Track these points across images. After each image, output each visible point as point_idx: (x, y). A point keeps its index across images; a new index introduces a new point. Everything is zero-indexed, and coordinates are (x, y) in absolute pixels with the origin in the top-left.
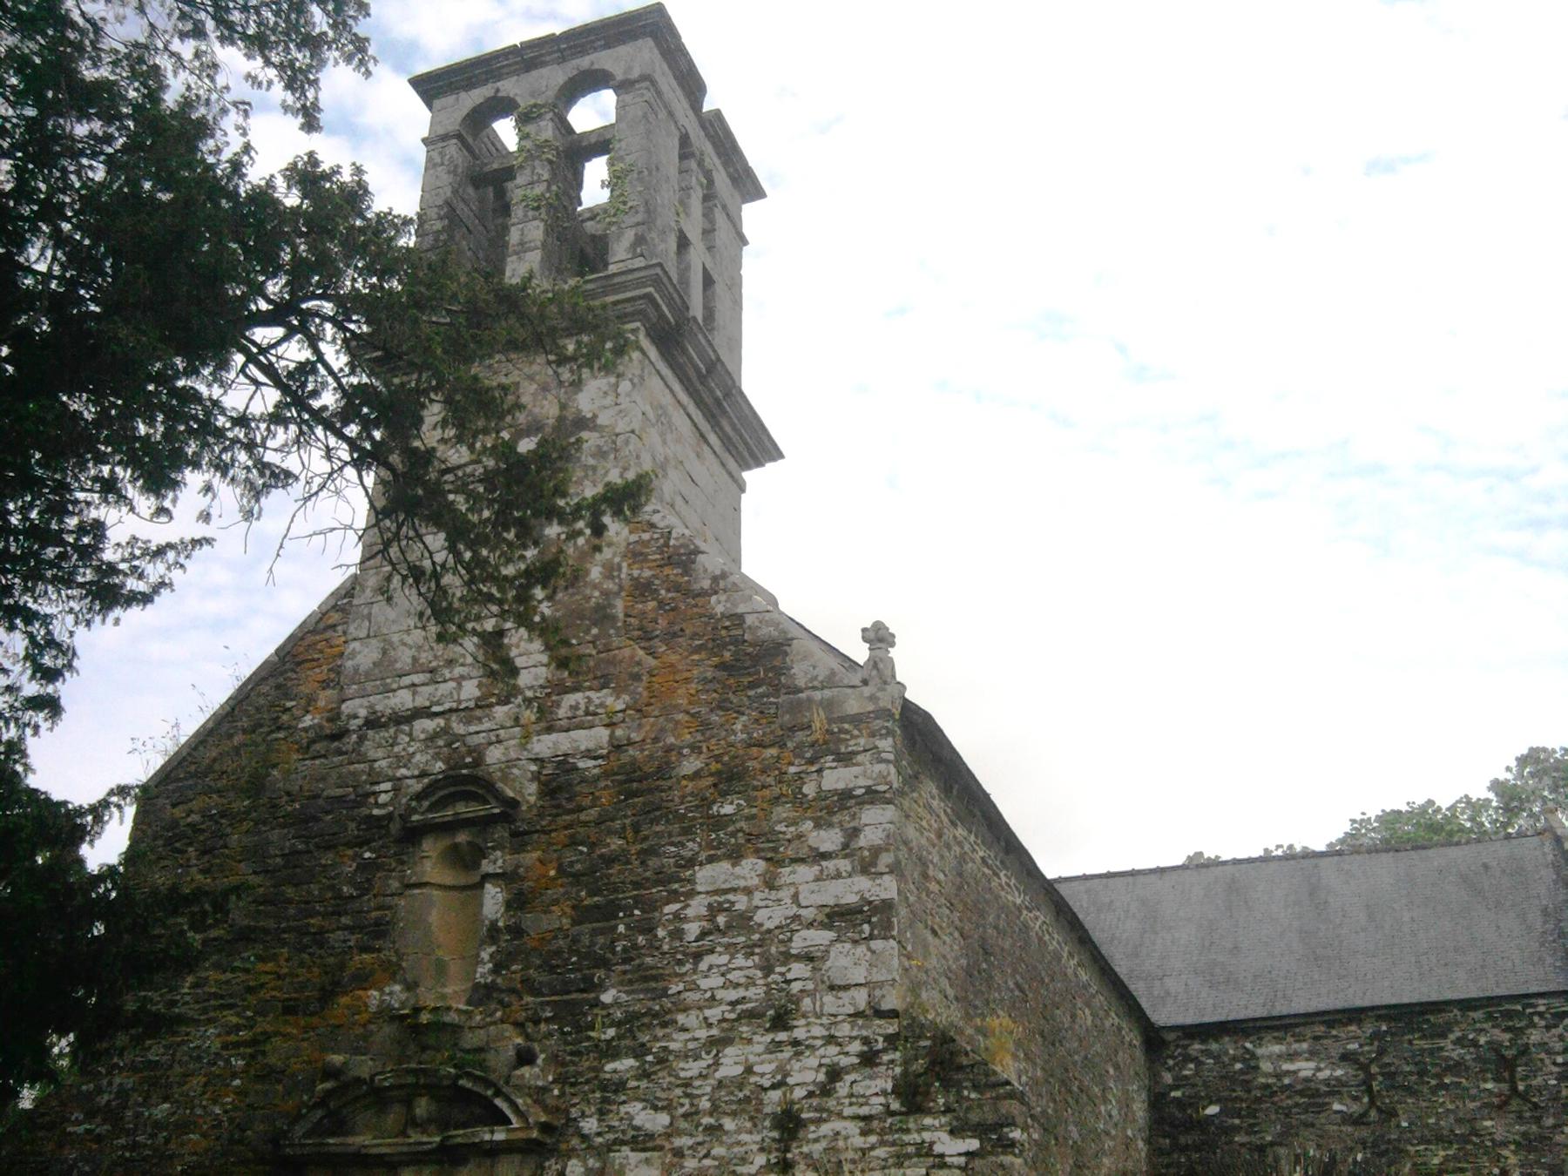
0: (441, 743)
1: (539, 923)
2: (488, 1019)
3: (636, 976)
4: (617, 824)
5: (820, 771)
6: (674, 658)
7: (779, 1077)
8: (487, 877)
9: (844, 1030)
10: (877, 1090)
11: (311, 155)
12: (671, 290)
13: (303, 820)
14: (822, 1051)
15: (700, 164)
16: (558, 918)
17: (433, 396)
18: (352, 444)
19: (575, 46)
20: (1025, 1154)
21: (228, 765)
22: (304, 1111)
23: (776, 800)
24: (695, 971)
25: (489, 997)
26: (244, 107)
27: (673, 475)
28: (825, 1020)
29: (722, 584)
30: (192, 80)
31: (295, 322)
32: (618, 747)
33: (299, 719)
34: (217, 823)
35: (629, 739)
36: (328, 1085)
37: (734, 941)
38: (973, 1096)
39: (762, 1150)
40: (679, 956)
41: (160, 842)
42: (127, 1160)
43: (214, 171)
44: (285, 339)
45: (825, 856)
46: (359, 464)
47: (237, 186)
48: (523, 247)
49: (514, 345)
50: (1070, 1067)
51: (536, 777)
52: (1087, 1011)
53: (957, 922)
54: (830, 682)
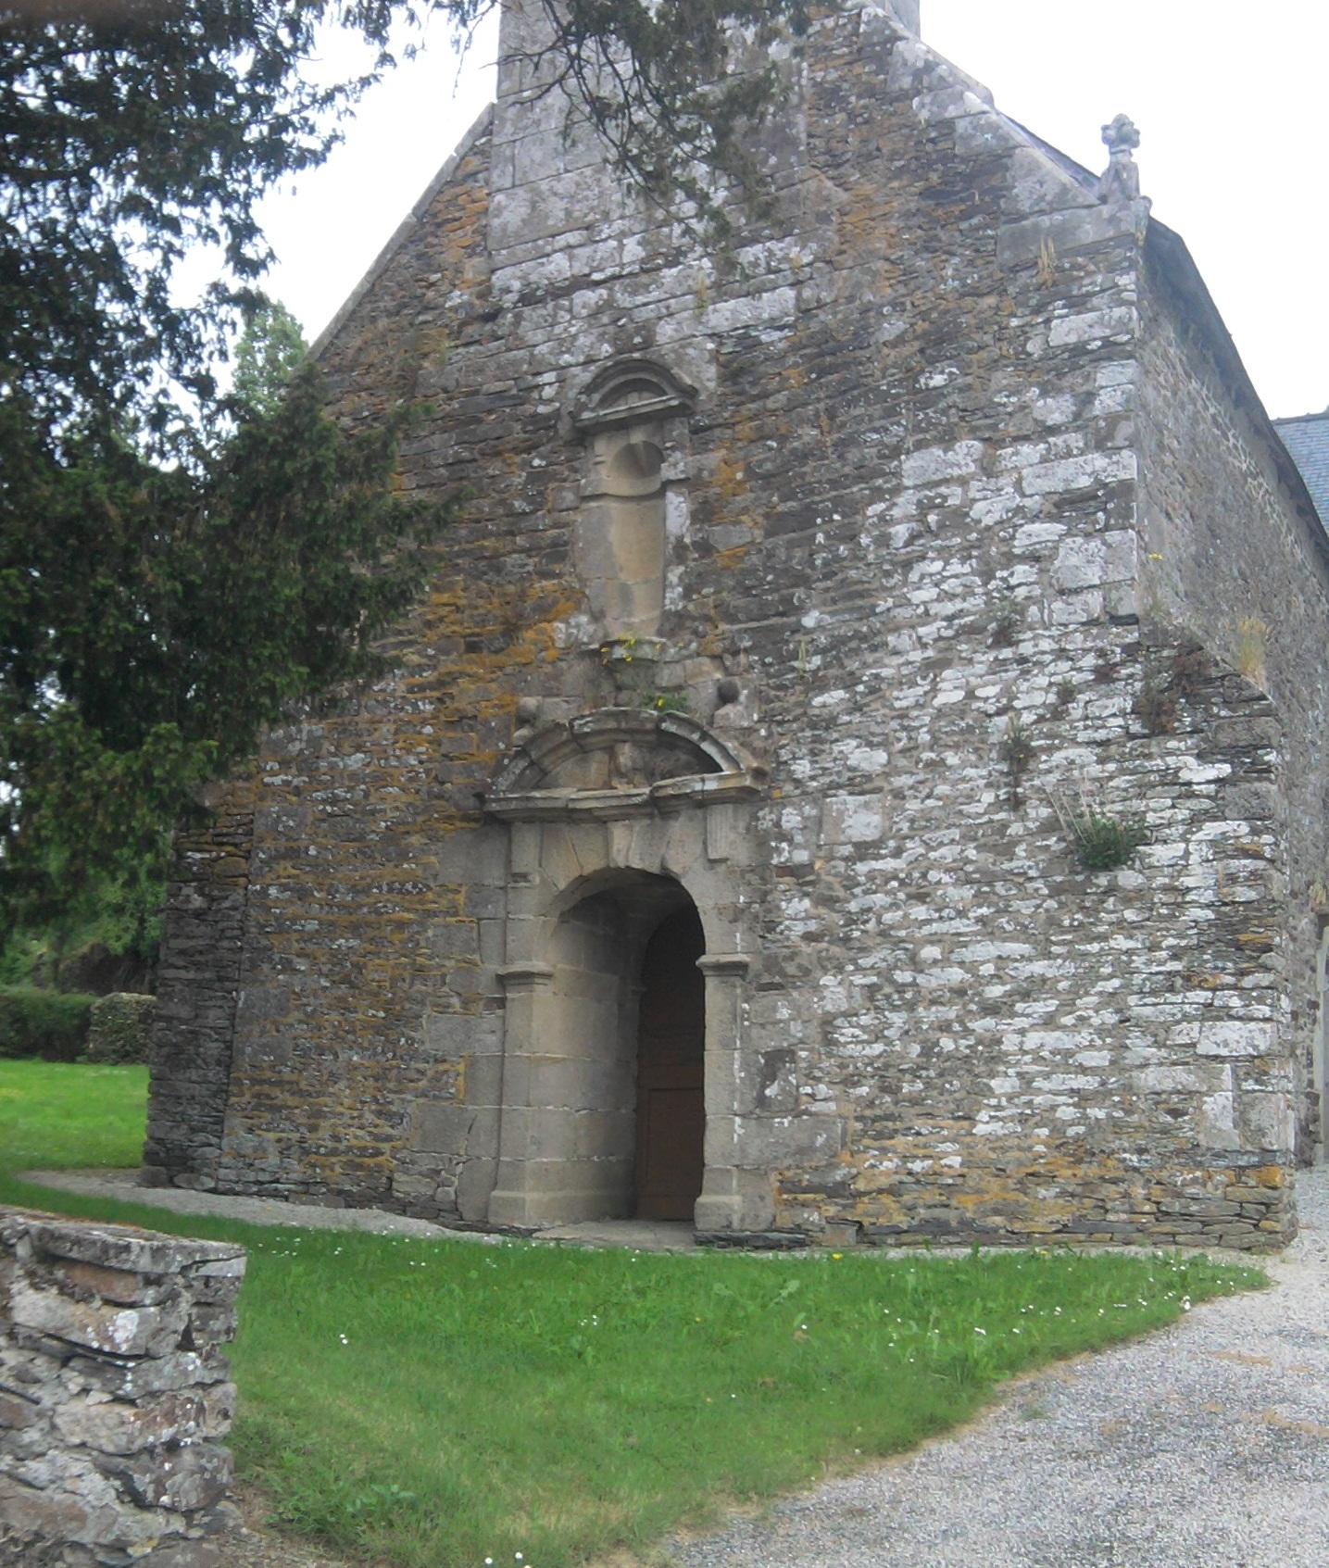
0: (605, 320)
5: (1047, 321)
6: (868, 188)
7: (1004, 701)
8: (667, 484)
10: (1114, 710)
13: (463, 423)
14: (1051, 668)
21: (373, 355)
23: (994, 365)
24: (905, 583)
25: (681, 626)
33: (445, 295)
35: (819, 300)
36: (524, 732)
38: (1223, 713)
39: (989, 785)
40: (886, 567)
42: (330, 815)
45: (1054, 430)
54: (1062, 200)
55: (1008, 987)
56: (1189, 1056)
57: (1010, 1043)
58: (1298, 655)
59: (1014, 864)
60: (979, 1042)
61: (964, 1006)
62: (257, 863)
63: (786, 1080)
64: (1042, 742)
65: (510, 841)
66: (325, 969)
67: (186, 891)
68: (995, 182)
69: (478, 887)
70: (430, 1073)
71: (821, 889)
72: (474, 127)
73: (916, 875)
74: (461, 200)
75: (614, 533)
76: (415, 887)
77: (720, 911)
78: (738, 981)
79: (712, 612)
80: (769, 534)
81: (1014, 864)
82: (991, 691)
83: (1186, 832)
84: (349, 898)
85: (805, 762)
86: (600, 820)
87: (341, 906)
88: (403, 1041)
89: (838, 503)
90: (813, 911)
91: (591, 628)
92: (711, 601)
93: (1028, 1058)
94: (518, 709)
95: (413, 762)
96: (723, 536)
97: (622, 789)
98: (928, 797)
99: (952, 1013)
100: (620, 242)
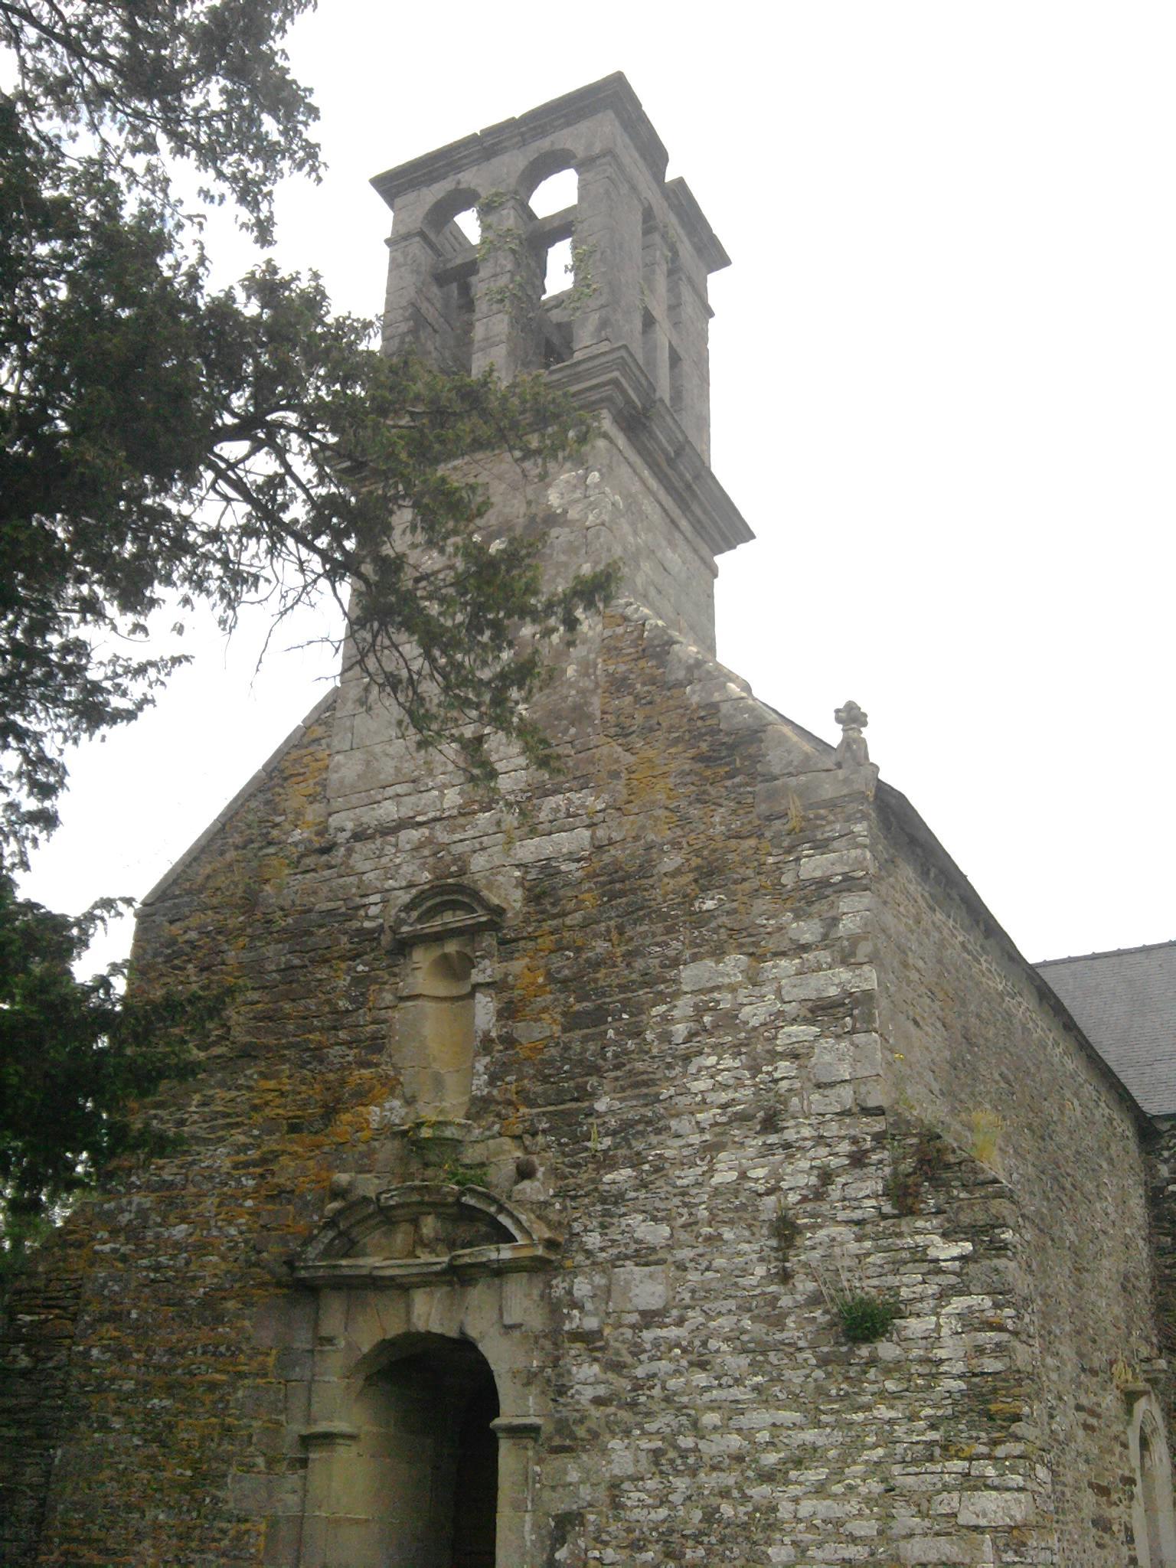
0: (426, 852)
1: (531, 1032)
2: (487, 1133)
3: (629, 1081)
4: (602, 927)
5: (798, 859)
6: (651, 753)
7: (773, 1182)
8: (476, 987)
9: (833, 1129)
10: (868, 1192)
11: (269, 262)
12: (638, 373)
13: (296, 935)
14: (811, 1153)
15: (664, 236)
16: (548, 1027)
17: (400, 502)
18: (326, 557)
19: (535, 128)
20: (1018, 1257)
21: (221, 881)
22: (315, 1232)
23: (755, 893)
24: (684, 1074)
25: (486, 1110)
26: (199, 220)
27: (646, 566)
28: (813, 1120)
29: (696, 674)
30: (146, 195)
31: (261, 435)
32: (600, 847)
33: (288, 833)
34: (214, 939)
35: (610, 839)
36: (335, 1205)
37: (721, 1041)
38: (962, 1195)
39: (761, 1260)
40: (669, 1060)
41: (160, 960)
42: (153, 1281)
43: (172, 285)
44: (253, 451)
45: (805, 948)
46: (334, 573)
47: (195, 299)
48: (489, 342)
49: (478, 445)
50: (1062, 1162)
51: (520, 883)
52: (1076, 1103)
53: (939, 1012)
54: (806, 766)
55: (782, 1455)
56: (951, 1527)
57: (785, 1511)
58: (1078, 1153)
59: (785, 1335)
60: (756, 1509)
61: (742, 1472)
62: (82, 1325)
63: (576, 1544)
64: (805, 1220)
65: (318, 1309)
66: (138, 1429)
67: (15, 1351)
68: (752, 750)
69: (287, 1350)
70: (232, 1533)
71: (610, 1355)
72: (320, 704)
73: (697, 1343)
74: (305, 760)
75: (430, 1029)
76: (228, 1349)
77: (515, 1374)
78: (530, 1444)
79: (514, 1097)
80: (566, 1030)
81: (785, 1335)
82: (760, 1173)
83: (937, 1306)
84: (165, 1360)
85: (596, 1234)
86: (402, 1287)
87: (158, 1368)
88: (208, 1500)
89: (625, 1004)
90: (602, 1377)
91: (403, 1111)
92: (513, 1087)
93: (802, 1526)
94: (332, 1183)
95: (233, 1231)
96: (530, 1032)
97: (425, 1257)
98: (707, 1269)
99: (729, 1479)
100: (442, 792)
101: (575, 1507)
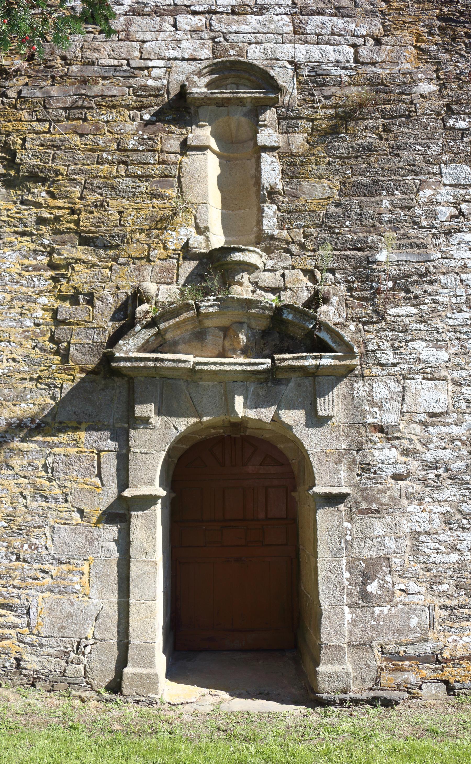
101: (382, 553)
